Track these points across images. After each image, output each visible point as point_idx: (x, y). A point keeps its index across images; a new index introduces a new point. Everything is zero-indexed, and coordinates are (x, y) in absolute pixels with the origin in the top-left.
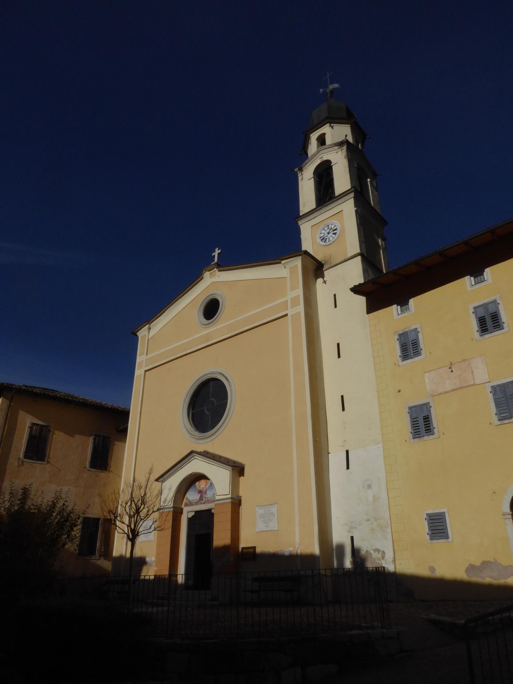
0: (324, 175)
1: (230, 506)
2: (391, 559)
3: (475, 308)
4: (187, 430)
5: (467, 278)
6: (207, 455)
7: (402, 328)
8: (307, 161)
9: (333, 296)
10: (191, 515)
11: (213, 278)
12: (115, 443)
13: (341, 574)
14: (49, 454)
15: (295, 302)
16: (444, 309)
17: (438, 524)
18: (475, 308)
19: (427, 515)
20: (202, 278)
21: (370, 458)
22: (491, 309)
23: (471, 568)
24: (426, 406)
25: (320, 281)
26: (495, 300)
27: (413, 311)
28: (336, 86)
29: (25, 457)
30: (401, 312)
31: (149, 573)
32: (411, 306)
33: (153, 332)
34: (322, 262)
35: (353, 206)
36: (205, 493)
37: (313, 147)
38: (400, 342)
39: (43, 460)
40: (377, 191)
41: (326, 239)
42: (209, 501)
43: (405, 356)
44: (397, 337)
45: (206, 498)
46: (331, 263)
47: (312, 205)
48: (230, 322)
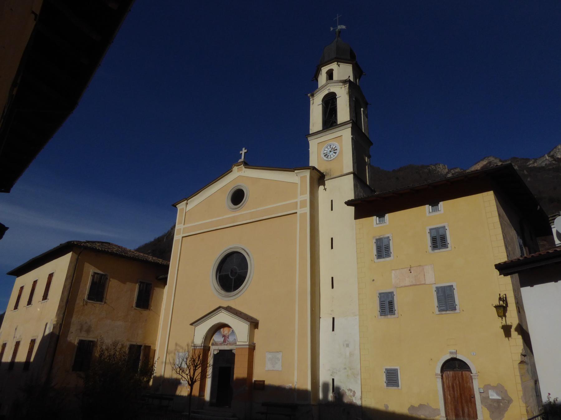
0: (330, 102)
2: (359, 397)
3: (430, 230)
5: (427, 206)
6: (229, 309)
7: (378, 235)
10: (216, 352)
12: (155, 288)
16: (409, 225)
18: (430, 230)
19: (386, 369)
21: (349, 326)
22: (441, 232)
23: (412, 408)
24: (392, 293)
25: (321, 188)
26: (445, 227)
28: (344, 27)
29: (89, 298)
31: (183, 391)
33: (189, 207)
36: (228, 338)
37: (322, 78)
38: (377, 245)
39: (101, 301)
43: (383, 312)
44: (374, 241)
48: (253, 210)
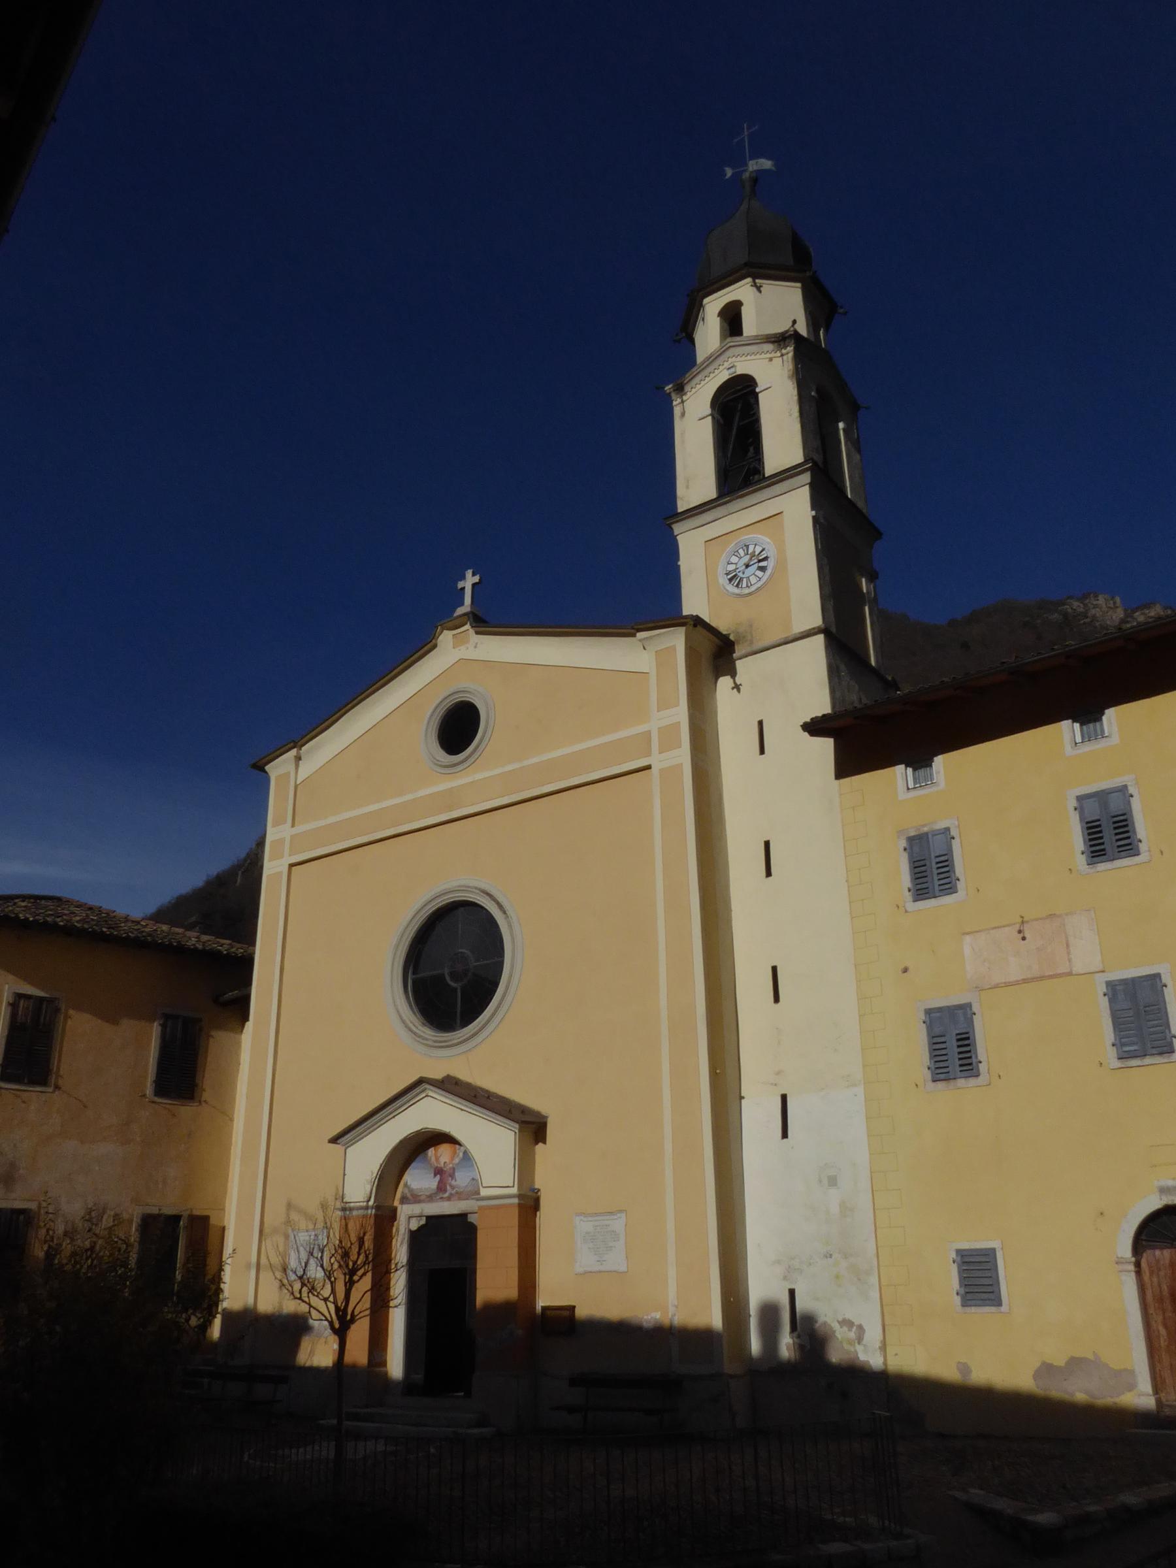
0: (737, 408)
1: (515, 1212)
3: (1080, 799)
4: (403, 1022)
5: (1066, 724)
6: (452, 1086)
7: (917, 823)
8: (694, 370)
9: (756, 724)
11: (463, 648)
13: (770, 1371)
14: (58, 1068)
15: (668, 739)
16: (1009, 789)
17: (980, 1274)
18: (1080, 799)
19: (958, 1251)
20: (435, 646)
21: (836, 1119)
22: (1115, 806)
23: (1046, 1370)
24: (964, 1012)
25: (725, 682)
26: (1125, 787)
27: (942, 785)
28: (766, 164)
30: (915, 783)
32: (938, 773)
33: (307, 769)
34: (732, 637)
35: (809, 509)
36: (452, 1176)
37: (708, 333)
39: (43, 1082)
40: (859, 451)
41: (741, 580)
42: (460, 1196)
43: (921, 891)
44: (903, 843)
45: (453, 1187)
46: (752, 642)
47: (711, 492)
